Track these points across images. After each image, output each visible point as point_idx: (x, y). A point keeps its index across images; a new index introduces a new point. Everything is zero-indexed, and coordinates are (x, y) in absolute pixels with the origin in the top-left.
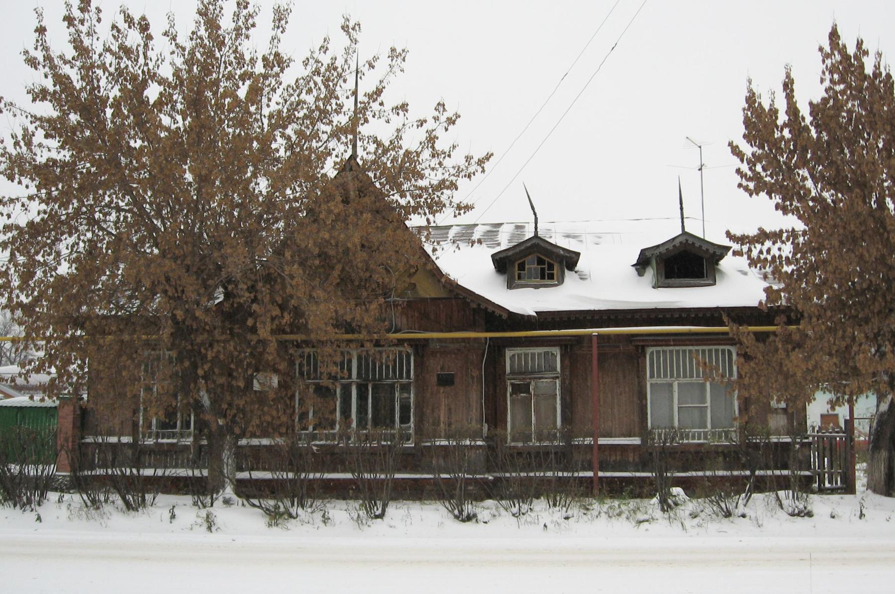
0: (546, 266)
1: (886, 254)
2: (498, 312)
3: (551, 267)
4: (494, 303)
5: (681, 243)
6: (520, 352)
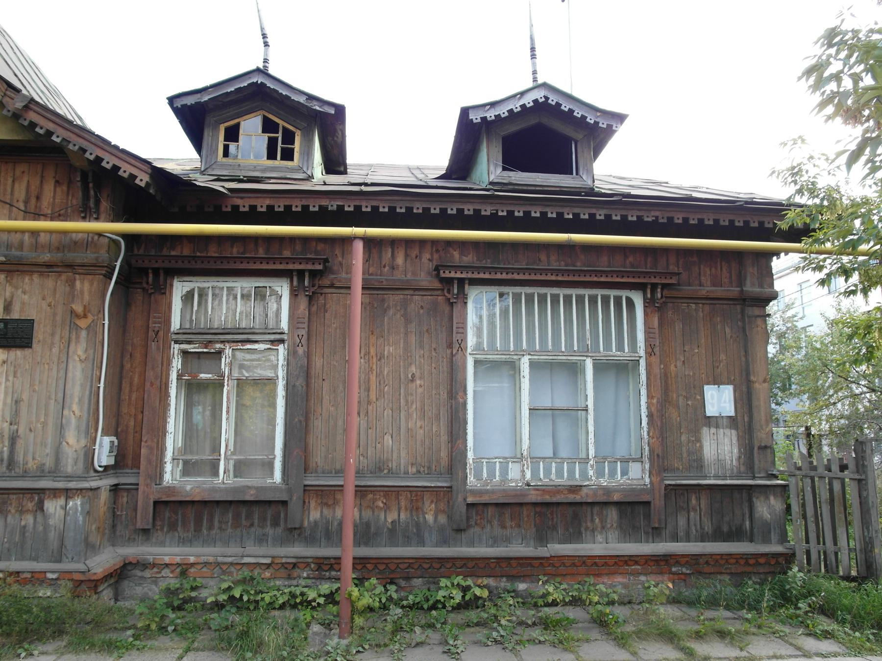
0: (280, 135)
1: (423, 603)
2: (126, 170)
3: (289, 138)
4: (116, 147)
5: (536, 101)
6: (206, 285)
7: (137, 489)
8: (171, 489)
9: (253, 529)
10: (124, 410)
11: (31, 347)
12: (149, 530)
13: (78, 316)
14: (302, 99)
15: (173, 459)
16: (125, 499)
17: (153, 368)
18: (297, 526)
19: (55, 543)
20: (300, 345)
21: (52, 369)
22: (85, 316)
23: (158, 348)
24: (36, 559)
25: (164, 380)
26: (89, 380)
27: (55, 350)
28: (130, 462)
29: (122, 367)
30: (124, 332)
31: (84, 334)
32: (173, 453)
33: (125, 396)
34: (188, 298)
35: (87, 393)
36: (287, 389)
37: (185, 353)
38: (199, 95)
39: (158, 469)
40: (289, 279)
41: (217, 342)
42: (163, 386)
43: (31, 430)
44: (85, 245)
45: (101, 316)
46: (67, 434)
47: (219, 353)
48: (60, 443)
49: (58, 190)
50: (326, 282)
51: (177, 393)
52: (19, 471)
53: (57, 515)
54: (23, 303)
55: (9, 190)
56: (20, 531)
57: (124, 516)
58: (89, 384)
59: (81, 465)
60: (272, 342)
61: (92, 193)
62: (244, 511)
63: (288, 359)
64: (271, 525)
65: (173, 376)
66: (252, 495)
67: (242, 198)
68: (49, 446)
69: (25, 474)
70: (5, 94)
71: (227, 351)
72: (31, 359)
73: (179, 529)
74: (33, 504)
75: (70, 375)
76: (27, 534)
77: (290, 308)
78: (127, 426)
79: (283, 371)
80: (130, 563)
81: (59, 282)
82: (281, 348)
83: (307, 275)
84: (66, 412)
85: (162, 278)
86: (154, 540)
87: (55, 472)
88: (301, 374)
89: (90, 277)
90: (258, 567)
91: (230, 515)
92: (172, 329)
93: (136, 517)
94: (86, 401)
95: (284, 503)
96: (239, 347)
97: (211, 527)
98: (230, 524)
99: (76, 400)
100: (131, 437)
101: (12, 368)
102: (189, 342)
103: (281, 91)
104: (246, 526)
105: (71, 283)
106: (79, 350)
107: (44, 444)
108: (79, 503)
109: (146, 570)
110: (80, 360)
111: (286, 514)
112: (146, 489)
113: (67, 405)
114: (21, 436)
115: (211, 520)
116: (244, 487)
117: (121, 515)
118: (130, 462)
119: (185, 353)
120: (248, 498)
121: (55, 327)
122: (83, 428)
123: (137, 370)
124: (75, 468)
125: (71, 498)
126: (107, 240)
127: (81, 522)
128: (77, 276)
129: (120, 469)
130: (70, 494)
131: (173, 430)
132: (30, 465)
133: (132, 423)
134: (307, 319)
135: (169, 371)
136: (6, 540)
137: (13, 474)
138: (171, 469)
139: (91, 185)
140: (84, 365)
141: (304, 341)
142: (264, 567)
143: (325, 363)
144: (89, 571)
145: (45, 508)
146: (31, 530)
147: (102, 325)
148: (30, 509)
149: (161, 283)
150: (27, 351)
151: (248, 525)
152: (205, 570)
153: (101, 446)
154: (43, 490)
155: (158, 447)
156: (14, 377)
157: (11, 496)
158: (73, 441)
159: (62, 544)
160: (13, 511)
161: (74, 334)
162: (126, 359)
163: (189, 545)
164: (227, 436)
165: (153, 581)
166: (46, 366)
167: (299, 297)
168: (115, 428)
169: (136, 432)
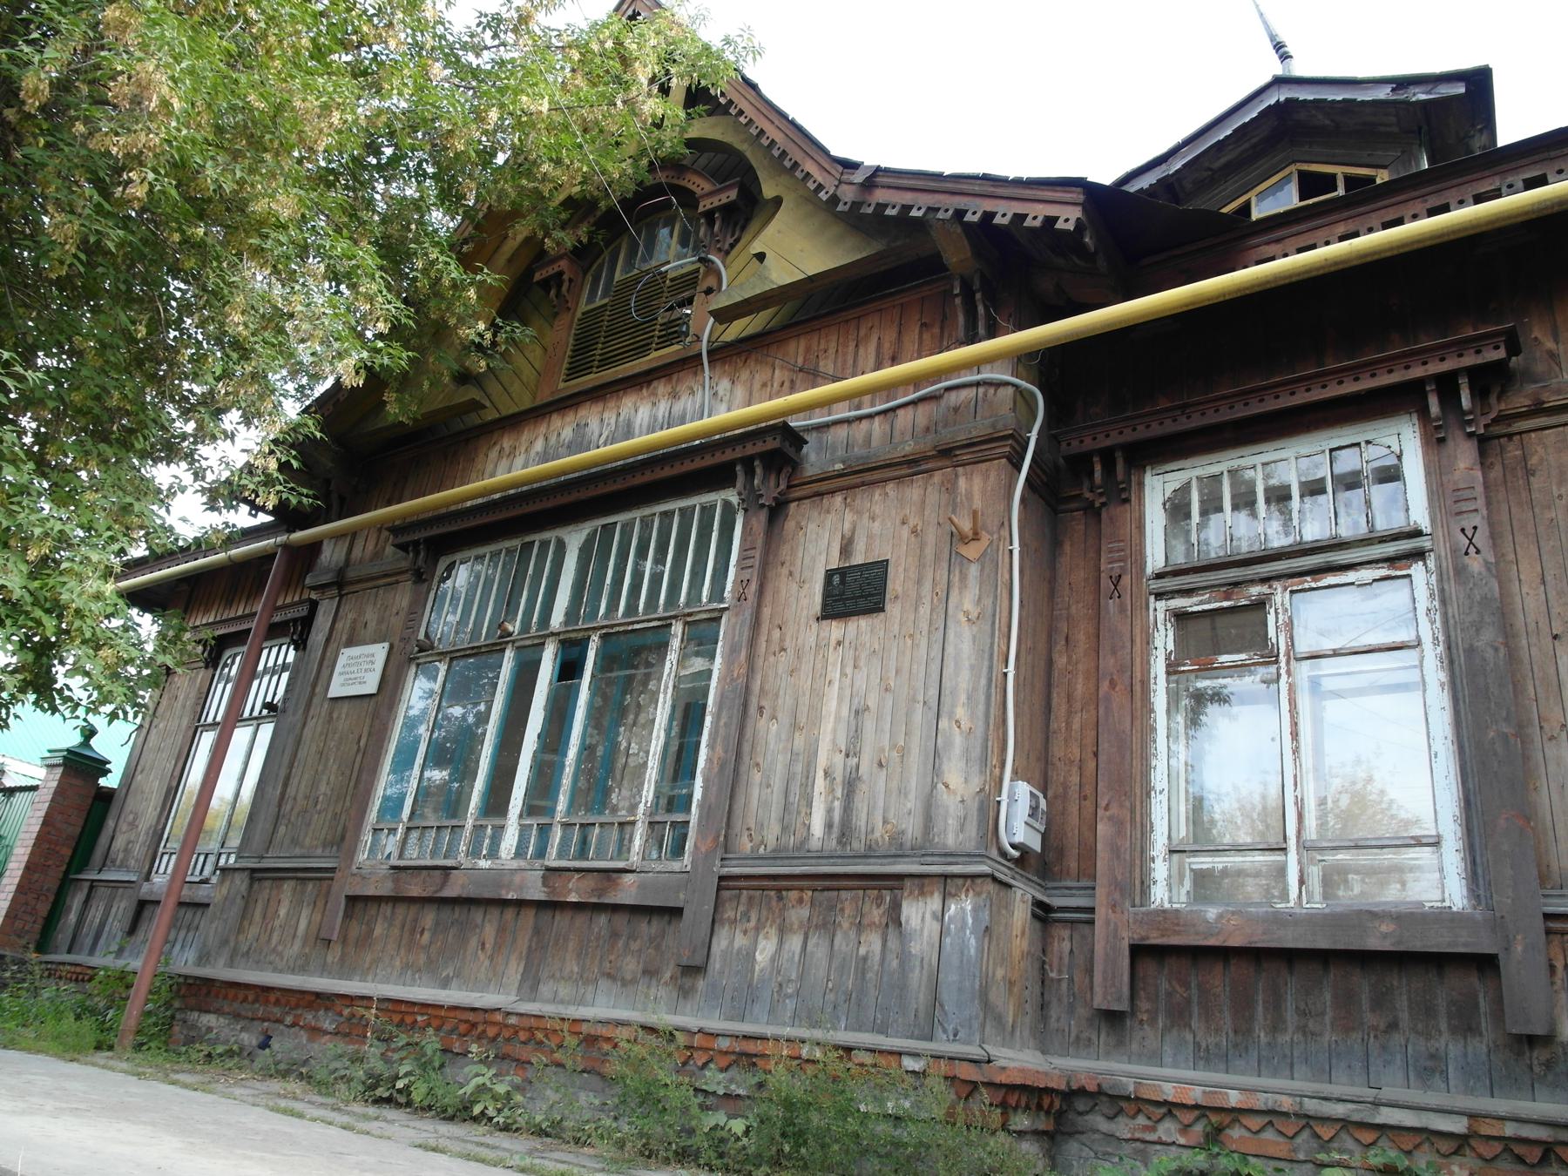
6: (1214, 470)
7: (1091, 922)
8: (1166, 917)
9: (1397, 1039)
10: (1057, 750)
11: (882, 610)
12: (1122, 1013)
13: (964, 540)
14: (1383, 93)
15: (1171, 852)
16: (1066, 946)
17: (1114, 652)
18: (1539, 1030)
19: (921, 996)
20: (1472, 550)
21: (918, 645)
22: (976, 537)
23: (1122, 610)
24: (882, 1030)
25: (1138, 675)
26: (986, 656)
27: (925, 610)
28: (1073, 865)
29: (1050, 663)
30: (1052, 594)
31: (974, 570)
32: (1169, 837)
33: (1058, 723)
34: (1177, 509)
35: (983, 682)
36: (1451, 662)
37: (1180, 617)
38: (1164, 166)
39: (1138, 870)
40: (1415, 417)
41: (1252, 582)
42: (1137, 688)
43: (880, 765)
44: (972, 410)
45: (1005, 533)
46: (945, 767)
47: (1260, 605)
48: (934, 786)
49: (926, 336)
50: (1519, 401)
51: (1168, 703)
52: (858, 846)
53: (926, 933)
54: (870, 537)
55: (850, 362)
56: (856, 968)
57: (1064, 985)
58: (986, 663)
59: (972, 830)
60: (1391, 560)
61: (981, 309)
62: (1366, 988)
63: (1442, 591)
64: (1454, 1030)
65: (1159, 667)
66: (1385, 936)
67: (1278, 241)
68: (912, 796)
69: (869, 853)
70: (840, 182)
71: (1278, 599)
72: (882, 633)
73: (1195, 1024)
74: (881, 910)
75: (950, 649)
76: (869, 975)
77: (1428, 473)
78: (1066, 787)
79: (1433, 622)
80: (1082, 1092)
81: (930, 489)
82: (1417, 570)
83: (1464, 383)
84: (943, 724)
85: (1120, 467)
86: (1135, 1046)
87: (921, 850)
88: (1488, 619)
89: (983, 466)
90: (1426, 1146)
91: (1328, 996)
92: (1149, 571)
93: (1092, 988)
94: (982, 698)
95: (1485, 964)
96: (1306, 586)
97: (1276, 1027)
98: (1327, 1019)
99: (963, 698)
100: (1073, 809)
101: (852, 652)
102: (1188, 592)
103: (1330, 98)
104: (1375, 1028)
105: (950, 488)
106: (967, 600)
107: (902, 792)
108: (969, 908)
109: (1120, 1119)
110: (969, 620)
111: (1498, 1001)
112: (1112, 916)
113: (945, 709)
114: (864, 778)
115: (1276, 1005)
116: (1360, 913)
117: (1059, 980)
118: (1073, 865)
119: (1180, 617)
120: (1374, 943)
121: (924, 566)
122: (976, 752)
123: (1080, 667)
124: (961, 836)
125: (954, 896)
126: (1010, 390)
127: (973, 951)
128: (960, 469)
129: (1054, 880)
130: (951, 888)
131: (1165, 785)
132: (877, 834)
133: (1075, 779)
134: (1480, 489)
135: (1149, 655)
136: (830, 985)
137: (848, 852)
138: (1165, 874)
139: (978, 296)
140: (975, 628)
141: (1481, 539)
142: (1445, 1146)
143: (1552, 594)
144: (989, 1061)
145: (903, 920)
146: (876, 968)
147: (1007, 552)
148: (877, 920)
149: (1120, 477)
150: (876, 620)
151: (1382, 1026)
152: (1269, 1135)
153: (1013, 800)
154: (900, 877)
155: (1133, 820)
156: (855, 667)
157: (844, 894)
158: (960, 782)
159: (935, 999)
160: (846, 925)
161: (957, 572)
162: (1059, 647)
163: (1223, 1066)
164: (1298, 793)
165: (1137, 1151)
166: (909, 642)
167: (1450, 443)
168: (1040, 770)
169: (1085, 798)
